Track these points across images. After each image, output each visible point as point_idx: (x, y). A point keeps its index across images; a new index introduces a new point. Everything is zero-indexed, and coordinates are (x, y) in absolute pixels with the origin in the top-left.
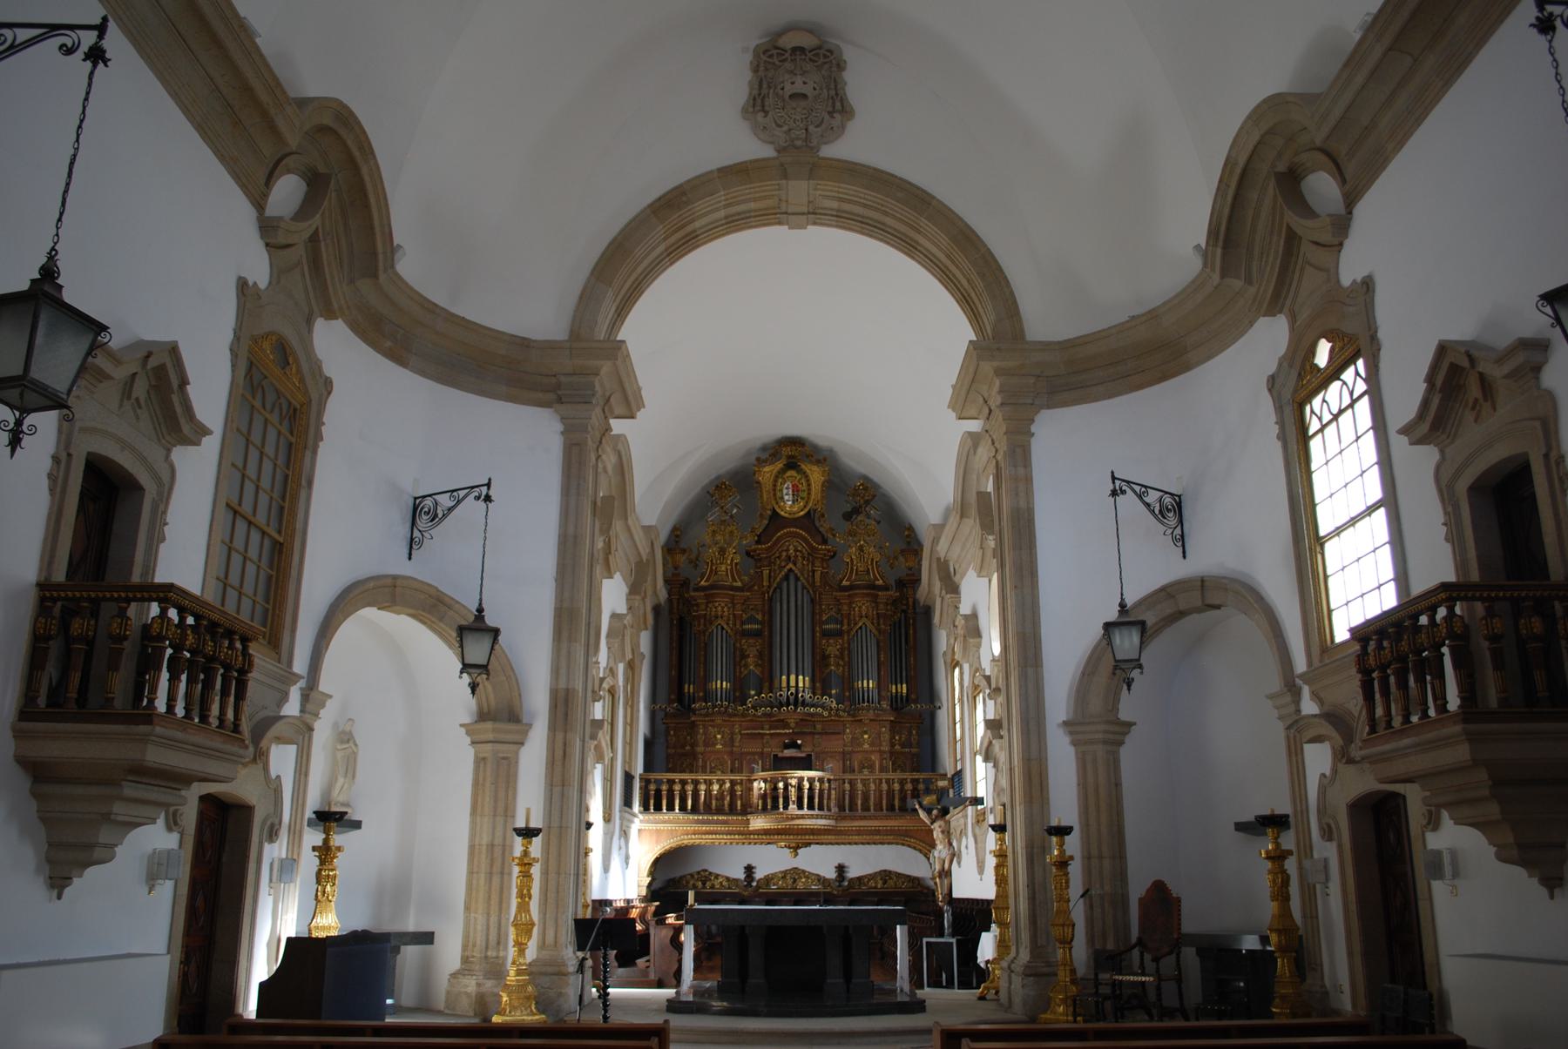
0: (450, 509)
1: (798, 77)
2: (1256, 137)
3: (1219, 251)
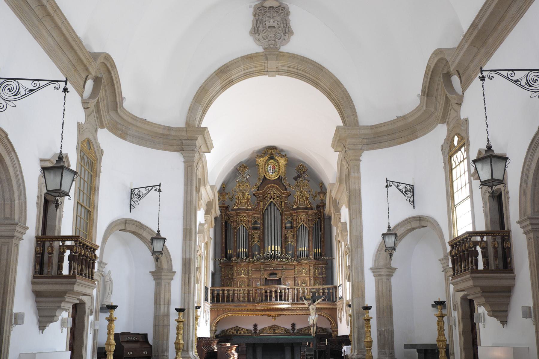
0: (145, 194)
1: (271, 18)
2: (436, 60)
3: (425, 97)
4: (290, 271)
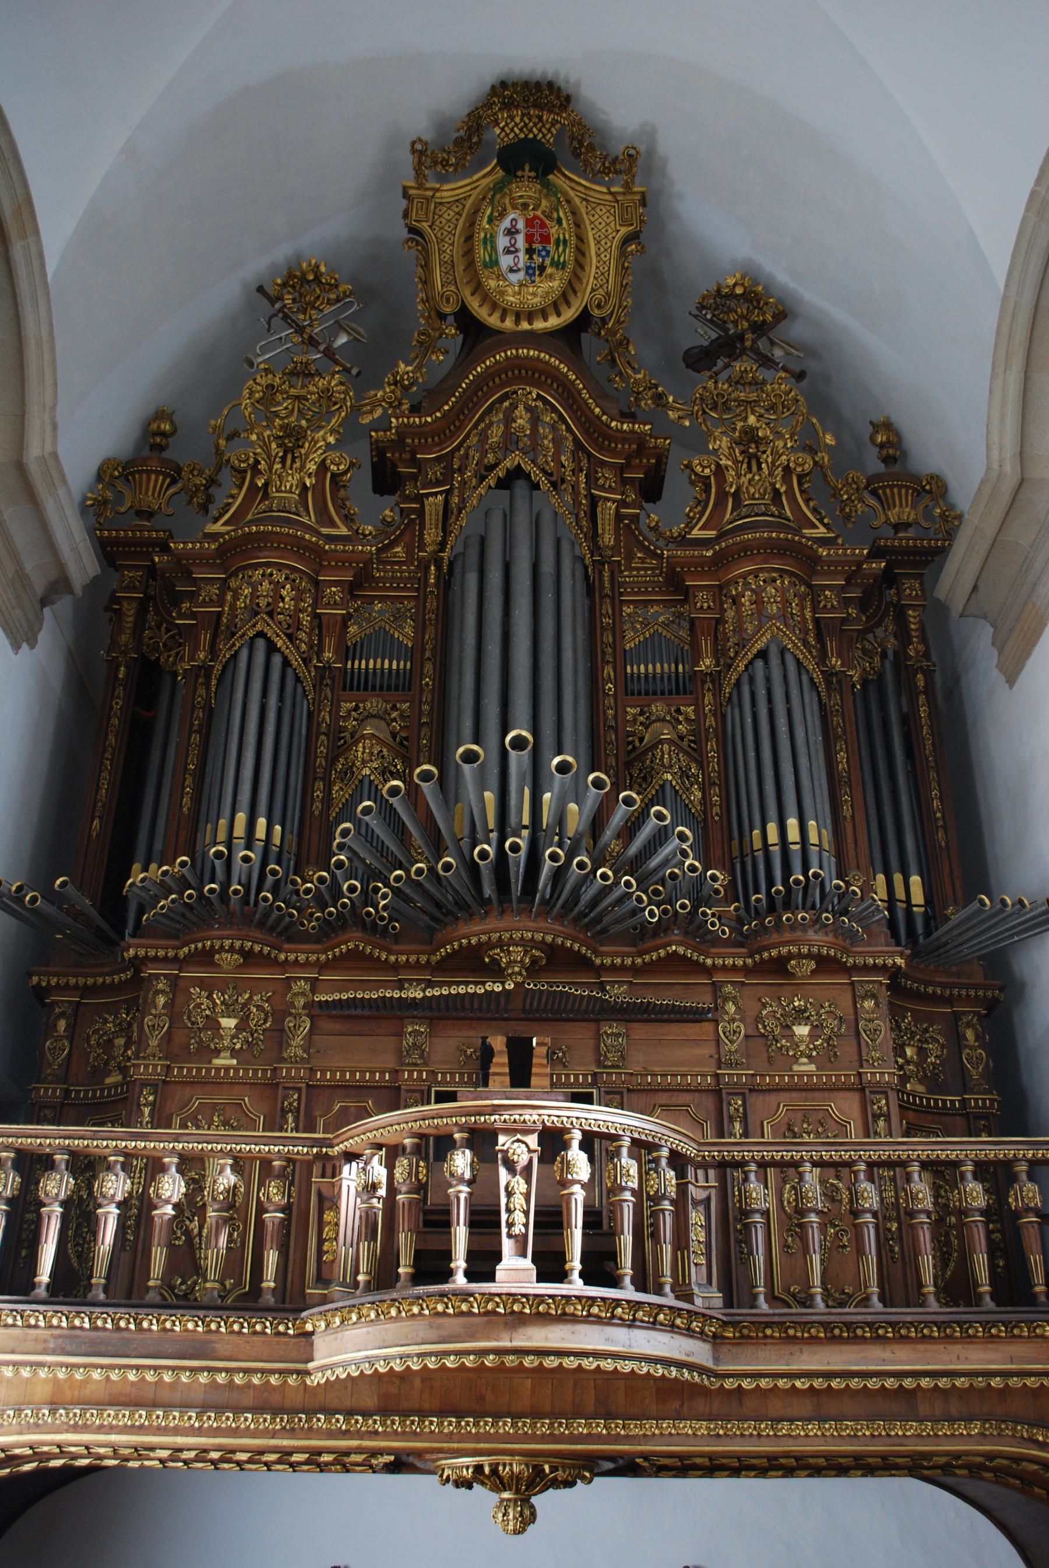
4: (674, 1031)
